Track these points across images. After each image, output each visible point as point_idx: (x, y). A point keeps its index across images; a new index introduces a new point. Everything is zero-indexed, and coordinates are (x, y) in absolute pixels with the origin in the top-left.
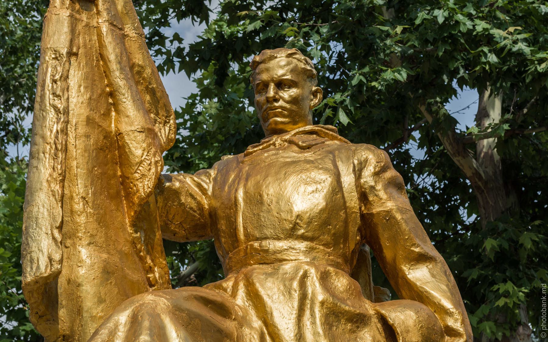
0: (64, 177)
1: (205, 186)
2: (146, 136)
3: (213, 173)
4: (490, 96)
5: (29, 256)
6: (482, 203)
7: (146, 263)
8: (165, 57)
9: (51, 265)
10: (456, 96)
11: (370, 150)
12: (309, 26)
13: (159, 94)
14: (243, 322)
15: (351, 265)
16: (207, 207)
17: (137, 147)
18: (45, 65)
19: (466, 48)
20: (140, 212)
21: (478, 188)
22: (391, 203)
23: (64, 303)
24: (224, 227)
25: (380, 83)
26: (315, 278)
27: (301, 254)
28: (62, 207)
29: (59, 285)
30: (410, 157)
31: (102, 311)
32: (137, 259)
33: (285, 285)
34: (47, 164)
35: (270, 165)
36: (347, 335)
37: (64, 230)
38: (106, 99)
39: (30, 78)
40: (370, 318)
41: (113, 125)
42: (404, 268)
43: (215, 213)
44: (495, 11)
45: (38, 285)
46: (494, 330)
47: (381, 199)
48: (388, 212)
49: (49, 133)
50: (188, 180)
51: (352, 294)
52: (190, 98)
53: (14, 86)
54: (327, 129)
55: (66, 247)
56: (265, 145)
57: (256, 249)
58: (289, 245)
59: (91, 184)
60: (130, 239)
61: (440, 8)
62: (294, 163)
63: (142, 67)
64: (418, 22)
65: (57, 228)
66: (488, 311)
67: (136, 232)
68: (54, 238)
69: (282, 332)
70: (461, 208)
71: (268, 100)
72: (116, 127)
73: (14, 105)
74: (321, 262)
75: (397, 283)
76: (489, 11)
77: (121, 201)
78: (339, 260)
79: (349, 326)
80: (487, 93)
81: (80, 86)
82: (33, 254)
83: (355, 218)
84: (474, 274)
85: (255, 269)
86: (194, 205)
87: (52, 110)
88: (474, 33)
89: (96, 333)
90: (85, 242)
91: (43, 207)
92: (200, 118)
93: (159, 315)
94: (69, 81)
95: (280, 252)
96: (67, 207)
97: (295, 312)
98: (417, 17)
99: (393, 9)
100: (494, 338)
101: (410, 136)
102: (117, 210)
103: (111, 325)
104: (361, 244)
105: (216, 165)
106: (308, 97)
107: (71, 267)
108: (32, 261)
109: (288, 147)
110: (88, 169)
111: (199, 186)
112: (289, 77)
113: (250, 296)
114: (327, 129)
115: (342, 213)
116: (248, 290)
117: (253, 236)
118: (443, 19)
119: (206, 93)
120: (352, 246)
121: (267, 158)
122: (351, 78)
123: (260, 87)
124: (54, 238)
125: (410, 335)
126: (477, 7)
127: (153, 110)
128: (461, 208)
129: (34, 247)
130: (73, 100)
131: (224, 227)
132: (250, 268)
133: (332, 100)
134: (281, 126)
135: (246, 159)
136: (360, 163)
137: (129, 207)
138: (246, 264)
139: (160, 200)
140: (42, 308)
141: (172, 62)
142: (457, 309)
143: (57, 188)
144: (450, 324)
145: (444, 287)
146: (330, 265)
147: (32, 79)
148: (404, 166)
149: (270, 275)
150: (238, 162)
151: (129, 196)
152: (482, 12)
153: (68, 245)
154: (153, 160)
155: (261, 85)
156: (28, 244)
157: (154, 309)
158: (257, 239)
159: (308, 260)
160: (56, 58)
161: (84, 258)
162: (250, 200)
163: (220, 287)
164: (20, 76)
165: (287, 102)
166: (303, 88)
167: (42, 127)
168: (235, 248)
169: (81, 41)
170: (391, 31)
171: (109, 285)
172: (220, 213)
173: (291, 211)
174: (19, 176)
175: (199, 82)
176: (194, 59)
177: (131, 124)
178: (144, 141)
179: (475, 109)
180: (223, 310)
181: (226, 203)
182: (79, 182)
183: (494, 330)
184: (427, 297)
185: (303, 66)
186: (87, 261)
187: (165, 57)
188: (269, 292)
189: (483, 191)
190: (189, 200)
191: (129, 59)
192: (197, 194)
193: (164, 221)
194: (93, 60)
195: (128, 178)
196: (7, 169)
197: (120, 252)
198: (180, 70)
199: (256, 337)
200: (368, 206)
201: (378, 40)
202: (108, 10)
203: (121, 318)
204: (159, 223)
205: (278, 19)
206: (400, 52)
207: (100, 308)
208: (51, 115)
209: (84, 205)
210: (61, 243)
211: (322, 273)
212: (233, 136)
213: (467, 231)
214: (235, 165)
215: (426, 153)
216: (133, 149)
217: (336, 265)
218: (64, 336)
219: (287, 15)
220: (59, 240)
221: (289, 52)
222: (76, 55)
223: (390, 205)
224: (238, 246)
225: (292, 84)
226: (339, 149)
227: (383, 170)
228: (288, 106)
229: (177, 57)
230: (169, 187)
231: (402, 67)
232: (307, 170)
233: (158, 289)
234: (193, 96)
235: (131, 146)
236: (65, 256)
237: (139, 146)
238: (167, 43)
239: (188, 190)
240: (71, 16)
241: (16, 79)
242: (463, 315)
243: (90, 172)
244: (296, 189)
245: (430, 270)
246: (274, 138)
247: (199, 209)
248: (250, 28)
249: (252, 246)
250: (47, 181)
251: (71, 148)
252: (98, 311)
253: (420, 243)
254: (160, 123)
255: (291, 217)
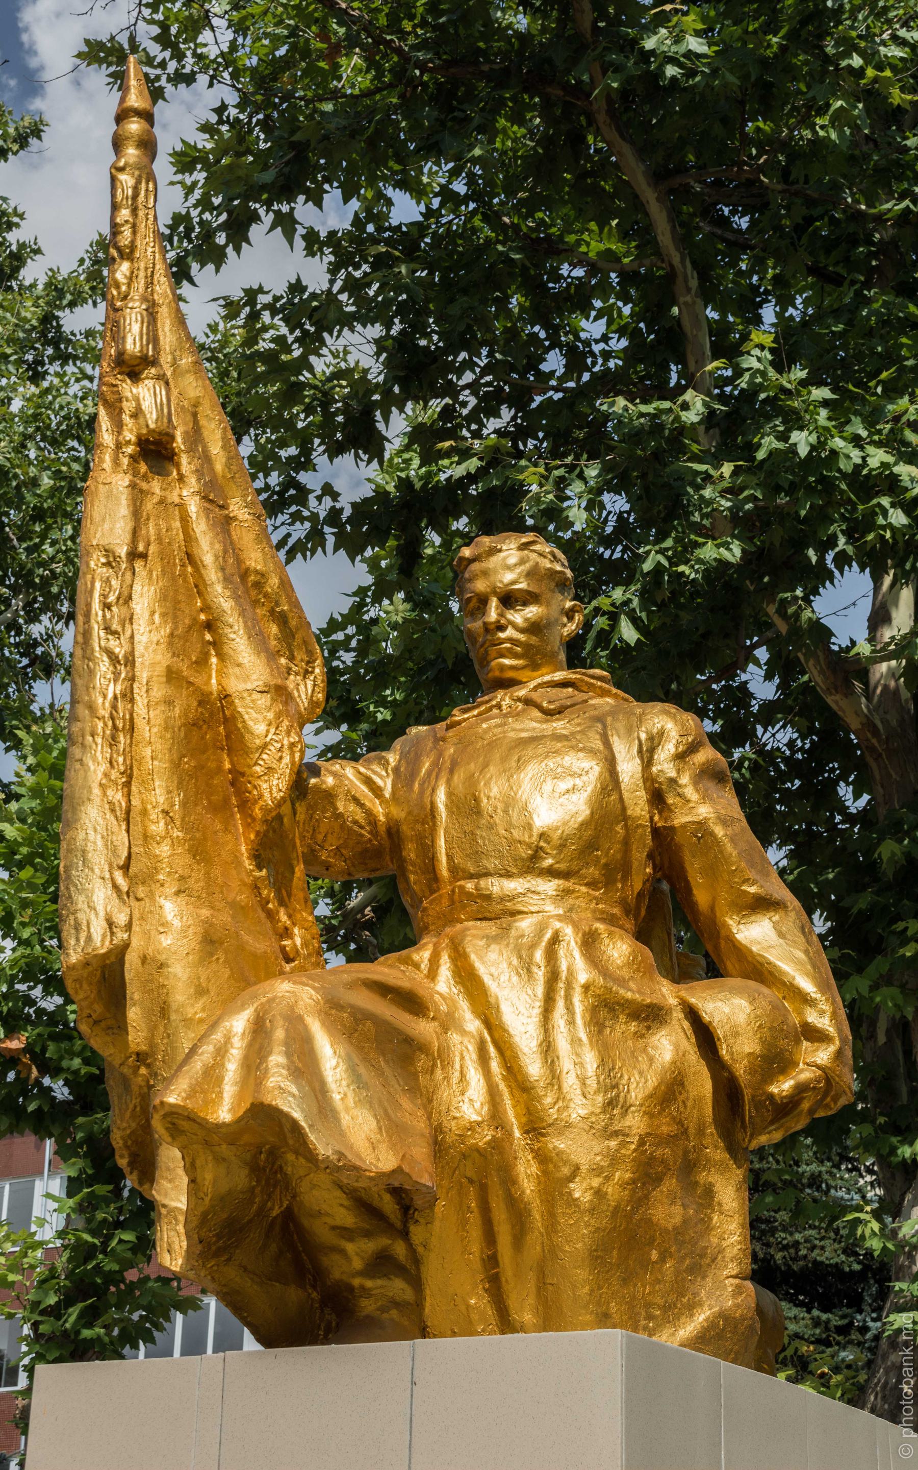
0: (130, 777)
1: (380, 782)
2: (273, 700)
3: (392, 758)
4: (893, 585)
5: (72, 917)
6: (878, 777)
7: (279, 921)
8: (307, 525)
9: (112, 933)
10: (832, 583)
11: (667, 713)
12: (566, 466)
13: (293, 623)
14: (448, 1022)
15: (636, 917)
16: (382, 819)
17: (258, 720)
18: (89, 577)
19: (850, 499)
20: (266, 834)
21: (872, 749)
22: (706, 809)
23: (136, 996)
24: (412, 856)
25: (692, 567)
26: (573, 943)
27: (548, 902)
28: (128, 831)
29: (127, 965)
30: (751, 695)
31: (203, 1010)
32: (263, 915)
33: (520, 957)
34: (99, 754)
35: (492, 745)
36: (630, 1043)
37: (132, 870)
38: (199, 636)
39: (70, 561)
40: (669, 1011)
41: (214, 681)
42: (730, 922)
43: (398, 831)
44: (902, 430)
45: (90, 969)
46: (900, 1001)
47: (688, 801)
48: (701, 824)
49: (100, 700)
50: (349, 772)
51: (638, 970)
52: (355, 594)
53: (42, 577)
54: (593, 677)
55: (138, 900)
56: (483, 708)
57: (469, 895)
58: (527, 885)
59: (180, 786)
60: (249, 881)
61: (801, 429)
62: (534, 740)
63: (263, 575)
64: (761, 455)
65: (120, 868)
66: (887, 967)
67: (259, 867)
68: (115, 887)
69: (517, 1039)
70: (842, 784)
71: (487, 628)
72: (219, 684)
73: (43, 610)
74: (583, 915)
75: (717, 947)
76: (892, 430)
77: (232, 815)
78: (616, 911)
79: (633, 1026)
80: (887, 580)
81: (153, 613)
82: (81, 916)
83: (643, 836)
84: (863, 902)
85: (468, 929)
86: (360, 816)
87: (105, 658)
88: (865, 472)
89: (193, 1051)
90: (171, 889)
91: (95, 830)
92: (375, 630)
93: (300, 1018)
94: (133, 605)
95: (512, 898)
96: (136, 829)
97: (538, 1004)
98: (759, 445)
99: (717, 430)
100: (898, 1016)
101: (749, 657)
102: (226, 830)
103: (218, 1036)
104: (654, 883)
105: (398, 744)
106: (557, 620)
107: (147, 934)
108: (77, 927)
109: (523, 710)
110: (172, 761)
111: (368, 782)
112: (522, 586)
113: (460, 976)
114: (593, 677)
115: (619, 828)
116: (456, 966)
117: (464, 871)
118: (808, 449)
119: (382, 590)
120: (638, 885)
121: (486, 731)
122: (642, 558)
123: (472, 605)
124: (115, 887)
125: (740, 1040)
126: (870, 422)
127: (284, 650)
128: (842, 784)
129: (80, 901)
130: (142, 639)
131: (412, 856)
132: (459, 926)
133: (608, 601)
134: (511, 674)
135: (451, 733)
136: (651, 738)
137: (247, 826)
138: (452, 921)
139: (301, 808)
140: (99, 1009)
141: (322, 534)
142: (823, 993)
143: (118, 796)
144: (810, 1020)
145: (801, 955)
146: (599, 920)
147: (73, 564)
148: (738, 712)
149: (496, 939)
150: (437, 740)
151: (245, 805)
152: (879, 432)
153: (141, 895)
154: (286, 742)
155: (475, 600)
156: (70, 897)
157: (292, 1008)
158: (471, 876)
159: (561, 912)
160: (108, 564)
161: (170, 917)
162: (458, 808)
163: (408, 961)
164: (52, 559)
165: (522, 631)
166: (548, 605)
167: (88, 688)
168: (432, 892)
169: (152, 531)
170: (712, 472)
171: (214, 965)
172: (405, 829)
173: (529, 826)
174: (56, 741)
175: (373, 565)
176: (362, 527)
177: (247, 678)
178: (269, 709)
179: (865, 608)
180: (412, 1002)
181: (415, 812)
182: (157, 783)
183: (900, 1001)
184: (771, 973)
185: (548, 565)
186: (171, 927)
187: (307, 525)
188: (493, 970)
189: (880, 755)
190: (352, 807)
191: (239, 561)
192: (366, 796)
193: (309, 846)
194: (175, 565)
195: (243, 774)
196: (34, 728)
197: (233, 905)
198: (336, 550)
199: (471, 1048)
200: (665, 814)
201: (690, 490)
202: (199, 473)
203: (235, 1023)
204: (300, 850)
205: (509, 454)
206: (729, 509)
207: (199, 1005)
208: (104, 666)
209: (166, 824)
210: (128, 894)
211: (584, 934)
212: (432, 663)
213: (853, 825)
214: (430, 744)
215: (778, 688)
216: (250, 723)
217: (610, 920)
218: (138, 1054)
219: (525, 446)
220: (125, 889)
221: (524, 540)
222: (144, 556)
223: (704, 811)
224: (439, 889)
225: (529, 598)
226: (613, 713)
227: (693, 748)
228: (522, 637)
229: (331, 526)
230: (315, 785)
231: (733, 536)
232: (557, 752)
233: (302, 969)
234: (361, 592)
235: (246, 717)
236: (136, 915)
237: (260, 717)
238: (312, 502)
239: (349, 791)
240: (133, 486)
241: (43, 564)
242: (834, 1003)
243: (176, 765)
244: (538, 788)
245: (775, 926)
246: (500, 694)
247: (370, 823)
248: (459, 471)
249: (462, 888)
250: (101, 785)
251: (140, 723)
252: (196, 1010)
253: (757, 877)
254: (297, 674)
255: (531, 836)
